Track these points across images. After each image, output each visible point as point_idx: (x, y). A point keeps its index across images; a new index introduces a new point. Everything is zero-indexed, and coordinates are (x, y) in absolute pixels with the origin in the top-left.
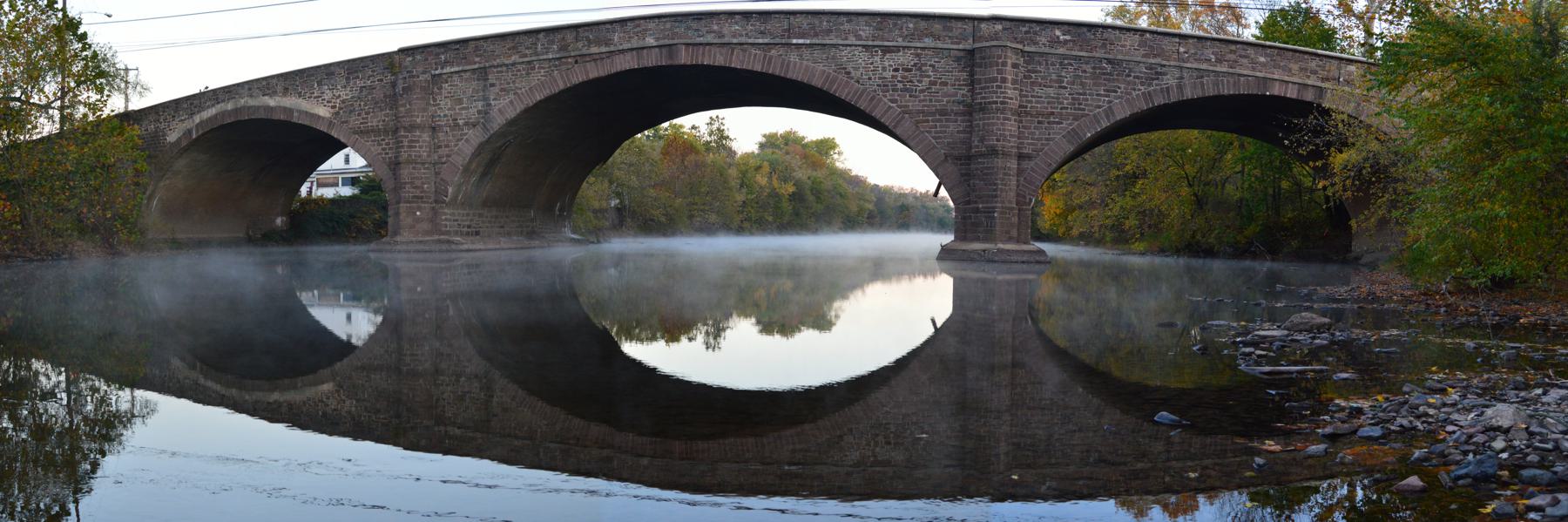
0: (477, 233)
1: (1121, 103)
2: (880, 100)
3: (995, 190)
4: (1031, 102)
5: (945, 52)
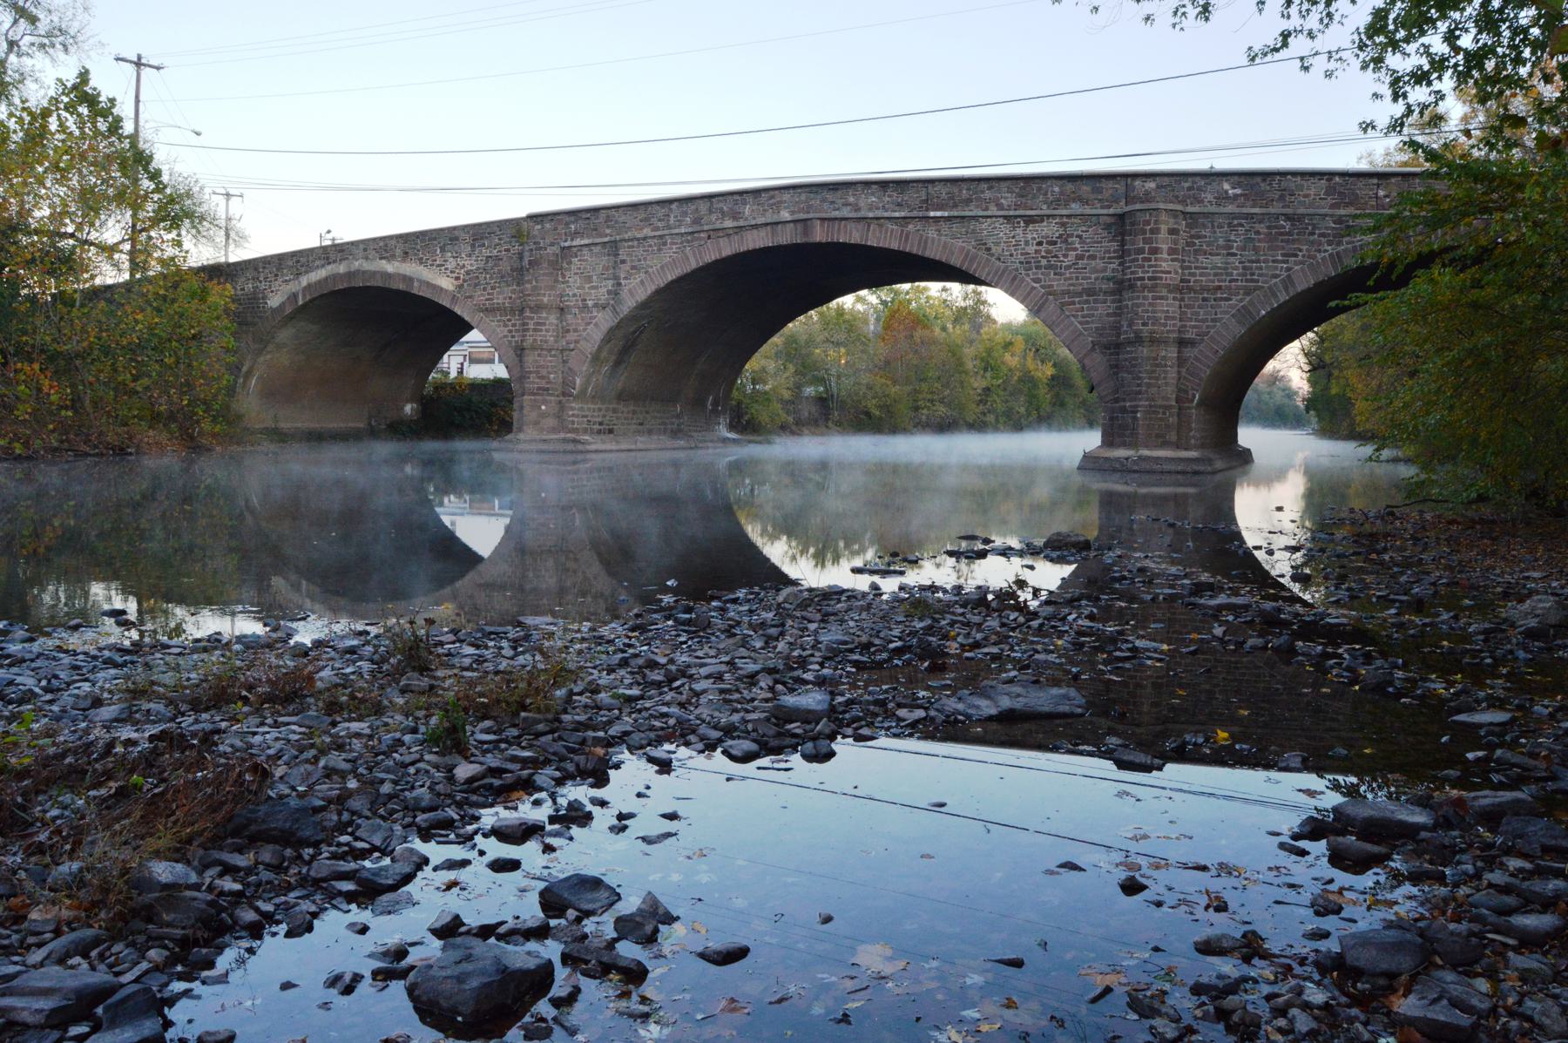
0: (611, 431)
1: (1302, 270)
2: (1023, 280)
3: (1139, 385)
4: (1194, 275)
5: (1094, 218)
